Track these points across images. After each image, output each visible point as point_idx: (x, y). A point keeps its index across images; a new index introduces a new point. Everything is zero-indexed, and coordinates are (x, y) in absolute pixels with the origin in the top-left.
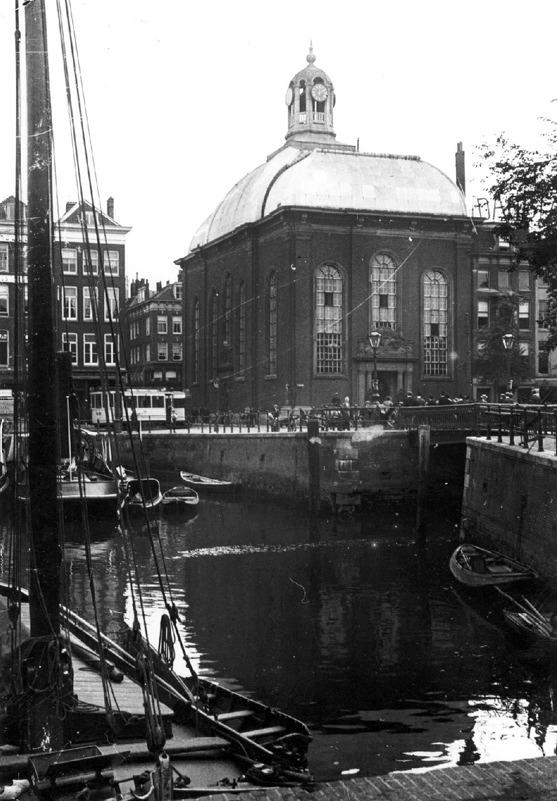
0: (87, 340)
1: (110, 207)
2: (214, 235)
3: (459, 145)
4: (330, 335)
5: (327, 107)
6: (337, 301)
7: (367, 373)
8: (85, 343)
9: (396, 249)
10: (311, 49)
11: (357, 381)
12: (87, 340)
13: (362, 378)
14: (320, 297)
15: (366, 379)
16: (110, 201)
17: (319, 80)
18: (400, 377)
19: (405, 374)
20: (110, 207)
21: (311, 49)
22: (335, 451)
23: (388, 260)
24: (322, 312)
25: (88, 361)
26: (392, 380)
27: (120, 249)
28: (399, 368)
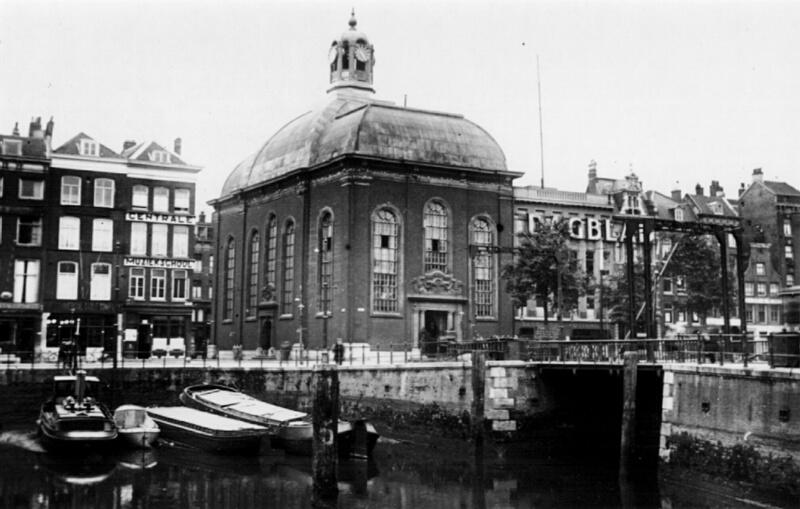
0: (133, 274)
1: (177, 148)
2: (258, 177)
3: (17, 124)
4: (386, 275)
5: (367, 67)
6: (392, 242)
7: (420, 312)
8: (152, 277)
9: (445, 196)
10: (353, 14)
11: (411, 319)
12: (133, 274)
13: (416, 316)
14: (378, 242)
15: (420, 317)
16: (178, 141)
17: (362, 42)
18: (450, 317)
19: (454, 314)
20: (177, 148)
21: (353, 14)
22: (694, 301)
23: (439, 208)
24: (379, 253)
25: (154, 295)
26: (441, 320)
27: (190, 188)
28: (450, 308)
